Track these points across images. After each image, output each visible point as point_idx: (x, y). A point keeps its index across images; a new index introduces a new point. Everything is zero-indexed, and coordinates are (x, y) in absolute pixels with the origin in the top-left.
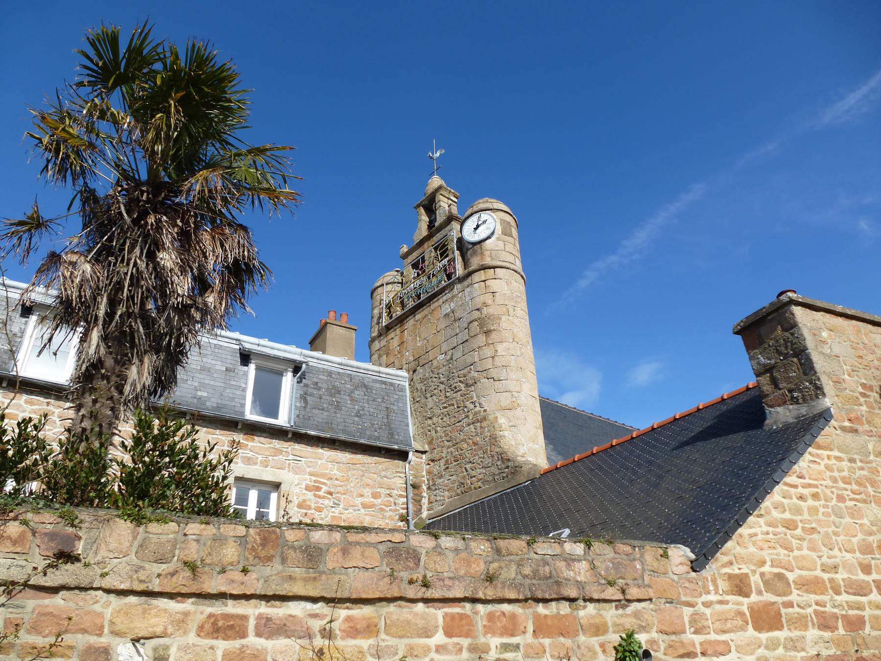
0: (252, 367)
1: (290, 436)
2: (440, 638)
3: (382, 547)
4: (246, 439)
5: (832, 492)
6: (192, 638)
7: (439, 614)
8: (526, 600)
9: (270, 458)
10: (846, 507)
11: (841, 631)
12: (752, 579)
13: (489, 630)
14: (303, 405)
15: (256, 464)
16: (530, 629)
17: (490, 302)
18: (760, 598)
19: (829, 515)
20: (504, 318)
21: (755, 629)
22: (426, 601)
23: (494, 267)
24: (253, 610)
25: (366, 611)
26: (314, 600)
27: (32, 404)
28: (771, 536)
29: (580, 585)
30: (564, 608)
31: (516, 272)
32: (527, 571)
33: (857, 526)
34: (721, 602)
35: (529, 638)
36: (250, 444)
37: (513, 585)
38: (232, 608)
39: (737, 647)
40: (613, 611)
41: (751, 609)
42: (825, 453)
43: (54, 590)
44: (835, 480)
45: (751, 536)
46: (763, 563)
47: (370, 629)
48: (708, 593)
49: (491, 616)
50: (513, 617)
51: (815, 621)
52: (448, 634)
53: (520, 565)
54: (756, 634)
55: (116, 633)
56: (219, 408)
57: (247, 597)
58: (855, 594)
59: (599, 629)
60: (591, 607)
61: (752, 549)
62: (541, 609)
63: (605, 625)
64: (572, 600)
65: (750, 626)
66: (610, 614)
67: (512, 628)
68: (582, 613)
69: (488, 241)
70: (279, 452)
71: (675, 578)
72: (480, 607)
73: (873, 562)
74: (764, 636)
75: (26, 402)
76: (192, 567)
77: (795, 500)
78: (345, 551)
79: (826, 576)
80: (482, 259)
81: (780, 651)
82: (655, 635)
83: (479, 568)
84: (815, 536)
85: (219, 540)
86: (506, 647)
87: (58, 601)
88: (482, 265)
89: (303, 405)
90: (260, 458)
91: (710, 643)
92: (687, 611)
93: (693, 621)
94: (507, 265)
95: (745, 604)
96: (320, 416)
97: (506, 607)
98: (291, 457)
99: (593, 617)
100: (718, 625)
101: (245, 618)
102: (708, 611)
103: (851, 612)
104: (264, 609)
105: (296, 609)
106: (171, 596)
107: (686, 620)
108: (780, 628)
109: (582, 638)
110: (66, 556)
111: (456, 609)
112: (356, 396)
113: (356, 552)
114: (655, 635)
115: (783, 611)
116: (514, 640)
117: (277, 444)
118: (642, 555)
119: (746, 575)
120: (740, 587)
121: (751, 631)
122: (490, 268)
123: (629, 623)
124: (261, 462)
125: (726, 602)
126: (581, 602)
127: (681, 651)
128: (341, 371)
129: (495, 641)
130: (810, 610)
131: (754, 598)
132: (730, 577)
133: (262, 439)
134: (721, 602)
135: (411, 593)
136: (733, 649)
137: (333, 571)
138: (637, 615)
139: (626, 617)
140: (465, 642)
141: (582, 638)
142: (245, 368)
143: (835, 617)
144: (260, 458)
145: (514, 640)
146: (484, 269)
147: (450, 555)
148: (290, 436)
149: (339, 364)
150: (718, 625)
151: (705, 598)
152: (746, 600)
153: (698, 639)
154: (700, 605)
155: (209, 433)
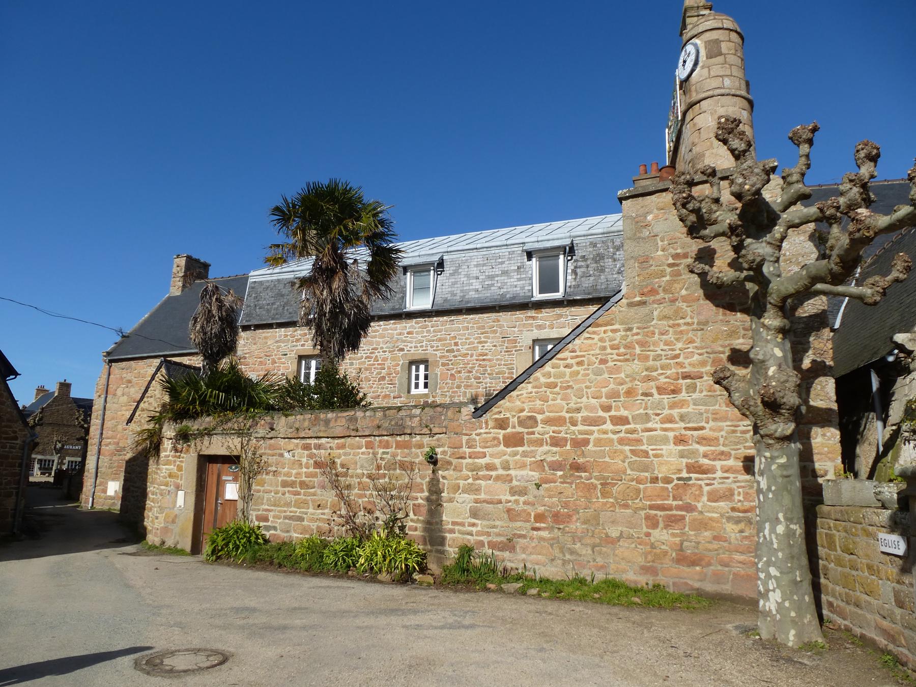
0: (534, 259)
1: (565, 303)
2: (364, 449)
3: (347, 418)
4: (537, 313)
5: (596, 358)
6: (300, 450)
7: (363, 441)
8: (393, 435)
9: (555, 322)
10: (607, 368)
11: (568, 447)
12: (511, 420)
13: (379, 447)
14: (574, 277)
15: (545, 328)
16: (394, 446)
17: (696, 141)
18: (514, 430)
19: (588, 375)
20: (707, 154)
21: (504, 446)
22: (359, 436)
23: (699, 102)
24: (313, 442)
25: (343, 440)
26: (328, 438)
27: (418, 323)
28: (534, 394)
29: (412, 428)
30: (407, 438)
31: (723, 95)
32: (393, 423)
33: (611, 380)
34: (486, 433)
35: (393, 450)
36: (540, 315)
37: (386, 429)
38: (308, 441)
39: (490, 455)
40: (428, 439)
41: (504, 436)
42: (603, 329)
43: (271, 438)
44: (604, 348)
45: (518, 396)
46: (522, 410)
47: (343, 446)
48: (481, 428)
49: (380, 441)
50: (387, 441)
51: (549, 442)
52: (366, 448)
53: (391, 420)
54: (505, 449)
55: (284, 450)
56: (514, 298)
57: (311, 438)
58: (589, 425)
59: (420, 446)
60: (418, 437)
61: (518, 403)
62: (398, 438)
63: (423, 444)
64: (410, 434)
65: (502, 445)
66: (426, 440)
67: (387, 445)
68: (414, 439)
69: (694, 75)
70: (560, 316)
71: (463, 422)
72: (377, 438)
73: (614, 404)
74: (509, 450)
75: (415, 323)
76: (297, 429)
77: (562, 368)
78: (336, 420)
79: (568, 415)
80: (690, 97)
81: (518, 457)
82: (446, 449)
83: (377, 422)
84: (569, 391)
85: (304, 420)
86: (384, 453)
87: (272, 441)
88: (689, 104)
89: (574, 277)
90: (548, 323)
91: (474, 453)
92: (465, 438)
93: (468, 442)
94: (710, 93)
95: (501, 433)
96: (587, 283)
97: (385, 438)
98: (570, 318)
99: (419, 441)
100: (482, 444)
101: (311, 444)
102: (477, 438)
103: (580, 436)
104: (316, 441)
105: (323, 441)
106: (294, 438)
107: (464, 442)
108: (522, 445)
109: (413, 450)
110: (272, 429)
111: (368, 439)
112: (618, 256)
113: (339, 421)
114: (446, 449)
115: (526, 436)
116: (388, 450)
117: (558, 311)
118: (447, 412)
119: (508, 418)
120: (502, 424)
121: (502, 447)
122: (696, 104)
123: (433, 443)
124: (549, 326)
125: (490, 433)
126: (413, 435)
127: (458, 456)
128: (605, 239)
129: (381, 451)
130: (547, 436)
131: (509, 430)
132: (496, 420)
133: (547, 310)
134: (486, 433)
135: (353, 433)
136: (487, 456)
137: (332, 428)
138: (438, 440)
139: (432, 441)
140: (371, 451)
141: (413, 450)
142: (530, 262)
143: (566, 440)
144: (548, 323)
145: (388, 450)
146: (691, 107)
147: (368, 418)
148: (565, 303)
149: (602, 234)
150: (482, 444)
151: (479, 431)
152: (503, 432)
153: (468, 450)
154: (474, 435)
155: (513, 315)
